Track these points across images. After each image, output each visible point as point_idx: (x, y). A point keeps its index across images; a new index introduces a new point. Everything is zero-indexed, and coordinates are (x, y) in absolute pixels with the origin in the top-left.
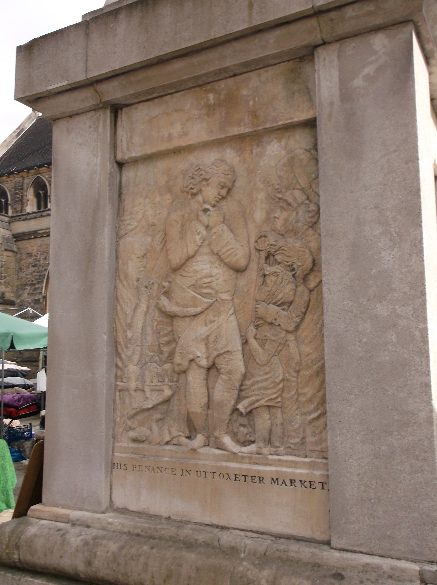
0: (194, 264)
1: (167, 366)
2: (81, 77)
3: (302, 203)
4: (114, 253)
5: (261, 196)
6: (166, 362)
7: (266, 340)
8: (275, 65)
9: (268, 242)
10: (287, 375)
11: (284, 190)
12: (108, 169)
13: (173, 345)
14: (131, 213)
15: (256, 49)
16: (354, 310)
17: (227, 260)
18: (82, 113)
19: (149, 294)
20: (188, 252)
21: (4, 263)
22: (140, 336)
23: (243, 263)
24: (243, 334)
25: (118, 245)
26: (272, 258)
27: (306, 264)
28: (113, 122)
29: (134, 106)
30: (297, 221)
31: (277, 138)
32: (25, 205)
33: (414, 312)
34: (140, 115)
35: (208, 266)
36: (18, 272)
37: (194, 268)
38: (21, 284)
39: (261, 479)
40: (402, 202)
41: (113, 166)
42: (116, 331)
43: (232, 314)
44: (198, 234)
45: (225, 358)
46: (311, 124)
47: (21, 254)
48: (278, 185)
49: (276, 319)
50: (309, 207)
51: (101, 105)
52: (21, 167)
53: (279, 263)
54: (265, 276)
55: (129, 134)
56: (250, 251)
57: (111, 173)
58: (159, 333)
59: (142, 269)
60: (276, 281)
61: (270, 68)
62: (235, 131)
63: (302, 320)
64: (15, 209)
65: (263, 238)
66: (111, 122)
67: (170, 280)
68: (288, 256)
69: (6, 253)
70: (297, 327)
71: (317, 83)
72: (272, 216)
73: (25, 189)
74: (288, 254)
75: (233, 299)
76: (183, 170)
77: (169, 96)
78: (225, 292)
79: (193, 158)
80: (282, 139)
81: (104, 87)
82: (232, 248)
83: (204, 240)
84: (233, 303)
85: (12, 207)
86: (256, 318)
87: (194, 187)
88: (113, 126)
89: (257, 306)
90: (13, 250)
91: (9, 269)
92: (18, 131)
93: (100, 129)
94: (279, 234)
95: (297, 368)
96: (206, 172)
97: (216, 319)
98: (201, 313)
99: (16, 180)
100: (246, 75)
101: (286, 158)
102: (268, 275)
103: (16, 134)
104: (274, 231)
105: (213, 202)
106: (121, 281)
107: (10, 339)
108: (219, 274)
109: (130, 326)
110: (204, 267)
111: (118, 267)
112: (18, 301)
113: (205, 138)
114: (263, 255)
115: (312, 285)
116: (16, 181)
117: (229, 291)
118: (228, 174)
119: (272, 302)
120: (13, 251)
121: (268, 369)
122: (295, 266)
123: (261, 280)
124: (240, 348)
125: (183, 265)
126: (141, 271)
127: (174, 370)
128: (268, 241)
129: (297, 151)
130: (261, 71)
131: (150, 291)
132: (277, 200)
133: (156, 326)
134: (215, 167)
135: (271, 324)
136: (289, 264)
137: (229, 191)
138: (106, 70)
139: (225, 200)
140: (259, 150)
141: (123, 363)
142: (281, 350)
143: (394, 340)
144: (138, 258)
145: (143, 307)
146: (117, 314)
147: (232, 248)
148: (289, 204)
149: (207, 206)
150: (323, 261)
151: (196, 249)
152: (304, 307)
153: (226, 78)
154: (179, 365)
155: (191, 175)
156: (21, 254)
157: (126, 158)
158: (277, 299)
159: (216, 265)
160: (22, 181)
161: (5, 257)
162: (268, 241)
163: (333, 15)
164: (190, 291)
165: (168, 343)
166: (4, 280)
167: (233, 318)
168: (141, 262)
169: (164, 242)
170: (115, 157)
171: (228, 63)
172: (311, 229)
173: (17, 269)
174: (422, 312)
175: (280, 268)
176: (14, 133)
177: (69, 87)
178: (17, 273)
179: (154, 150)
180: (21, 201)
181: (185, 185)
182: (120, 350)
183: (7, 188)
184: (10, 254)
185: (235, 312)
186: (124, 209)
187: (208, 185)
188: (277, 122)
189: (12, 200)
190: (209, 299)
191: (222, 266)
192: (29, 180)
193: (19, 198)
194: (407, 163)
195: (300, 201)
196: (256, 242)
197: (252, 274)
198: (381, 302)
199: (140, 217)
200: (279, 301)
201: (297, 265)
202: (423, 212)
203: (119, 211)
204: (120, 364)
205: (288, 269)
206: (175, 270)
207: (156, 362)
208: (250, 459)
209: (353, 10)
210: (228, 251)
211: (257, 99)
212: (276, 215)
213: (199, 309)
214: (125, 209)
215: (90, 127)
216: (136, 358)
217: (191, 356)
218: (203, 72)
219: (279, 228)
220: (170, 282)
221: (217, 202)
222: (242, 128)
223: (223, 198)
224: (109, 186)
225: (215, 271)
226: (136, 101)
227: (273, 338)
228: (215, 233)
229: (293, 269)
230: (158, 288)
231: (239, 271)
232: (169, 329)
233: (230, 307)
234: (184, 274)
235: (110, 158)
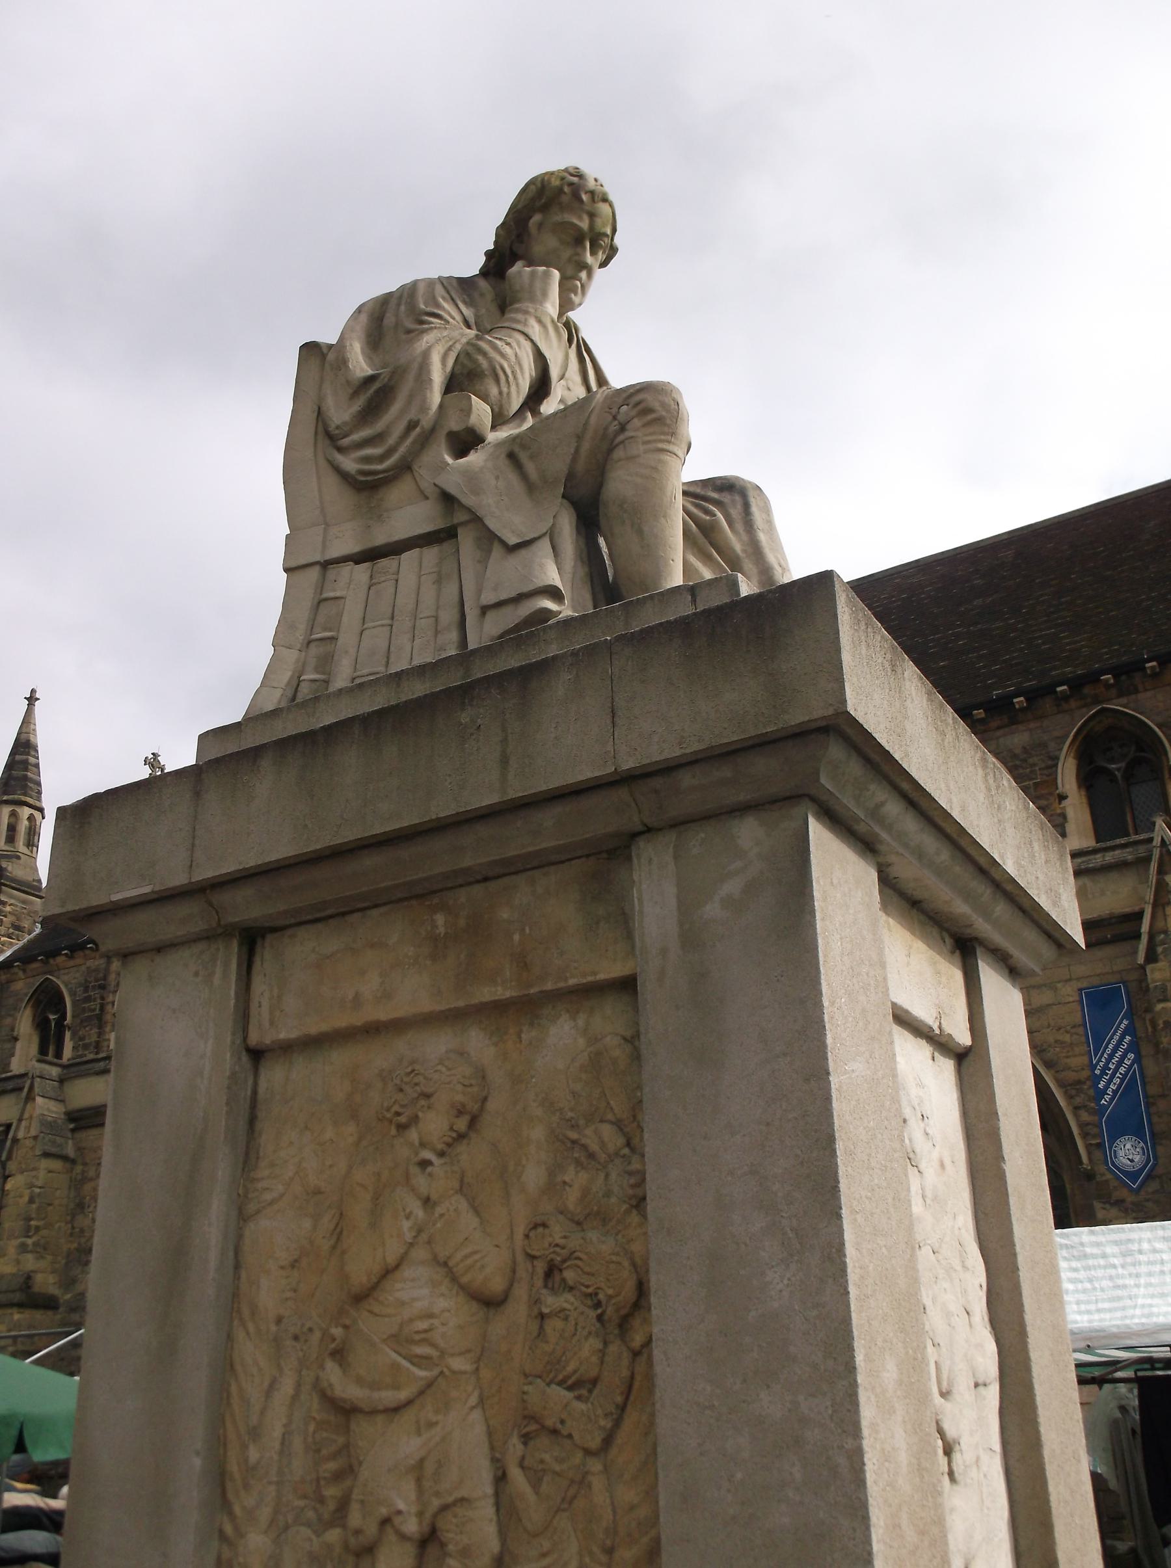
0: (398, 1286)
1: (334, 1535)
2: (179, 879)
3: (617, 1154)
4: (231, 1254)
5: (538, 1133)
6: (331, 1524)
7: (544, 1470)
8: (562, 862)
9: (550, 1239)
10: (587, 1560)
11: (582, 1122)
12: (228, 1066)
13: (348, 1483)
14: (272, 1165)
15: (519, 839)
16: (716, 1403)
17: (465, 1280)
18: (183, 944)
19: (301, 1354)
20: (384, 1258)
21: (37, 1190)
22: (276, 1457)
23: (497, 1285)
24: (498, 1455)
25: (240, 1236)
26: (557, 1277)
27: (623, 1294)
28: (245, 965)
29: (289, 932)
30: (608, 1194)
31: (568, 1011)
32: (108, 1029)
33: (834, 1411)
34: (303, 949)
35: (425, 1291)
36: (73, 1216)
37: (398, 1295)
38: (77, 1250)
40: (802, 1163)
41: (240, 1059)
42: (225, 1444)
43: (473, 1408)
44: (408, 1217)
45: (455, 1516)
46: (628, 985)
47: (85, 1164)
48: (572, 1110)
49: (562, 1422)
50: (630, 1163)
51: (220, 931)
53: (571, 1289)
54: (542, 1316)
55: (276, 991)
56: (514, 1256)
57: (233, 1076)
58: (318, 1451)
59: (289, 1294)
60: (563, 1330)
61: (553, 868)
62: (486, 994)
63: (617, 1423)
64: (81, 1039)
65: (540, 1230)
66: (239, 965)
67: (347, 1322)
68: (588, 1274)
69: (45, 1164)
70: (608, 1441)
71: (637, 908)
72: (559, 1179)
73: (112, 988)
74: (587, 1269)
75: (477, 1369)
76: (383, 1070)
77: (359, 914)
78: (461, 1354)
79: (402, 1046)
80: (578, 1012)
81: (224, 898)
82: (475, 1252)
83: (420, 1231)
84: (478, 1379)
85: (74, 1035)
86: (525, 1417)
87: (400, 1110)
88: (244, 973)
89: (526, 1388)
90: (64, 1152)
91: (51, 1208)
93: (217, 980)
94: (572, 1220)
95: (609, 1542)
96: (425, 1078)
97: (440, 1417)
98: (409, 1403)
99: (90, 963)
100: (506, 880)
101: (586, 1054)
102: (549, 1315)
104: (561, 1213)
105: (440, 1146)
106: (243, 1324)
107: (14, 1432)
108: (449, 1311)
109: (255, 1433)
110: (419, 1294)
111: (238, 1288)
112: (68, 1296)
113: (426, 1005)
114: (541, 1267)
115: (638, 1340)
116: (88, 968)
117: (469, 1351)
118: (471, 1085)
119: (556, 1380)
120: (64, 1158)
121: (546, 1545)
122: (601, 1296)
123: (534, 1327)
124: (490, 1490)
125: (375, 1287)
126: (287, 1299)
127: (346, 1546)
128: (551, 1235)
129: (608, 1038)
130: (536, 873)
131: (305, 1348)
132: (569, 1144)
133: (314, 1432)
134: (444, 1069)
135: (555, 1432)
136: (590, 1290)
137: (474, 1121)
138: (229, 867)
139: (465, 1141)
140: (533, 1034)
141: (236, 1528)
142: (575, 1497)
143: (798, 1476)
144: (282, 1268)
145: (287, 1387)
146: (229, 1404)
147: (475, 1252)
148: (592, 1156)
149: (427, 1155)
150: (653, 1290)
151: (402, 1251)
152: (622, 1393)
153: (470, 884)
154: (358, 1532)
155: (398, 1082)
156: (85, 1164)
157: (268, 1042)
158: (565, 1373)
159: (443, 1289)
160: (104, 966)
161: (42, 1174)
162: (551, 1235)
163: (657, 782)
164: (387, 1349)
165: (338, 1476)
166: (35, 1239)
167: (476, 1415)
168: (287, 1277)
169: (338, 1233)
170: (245, 1038)
171: (467, 861)
172: (635, 1212)
173: (72, 1206)
174: (849, 1411)
175: (572, 1299)
177: (156, 896)
178: (69, 1218)
179: (324, 1027)
180: (100, 1018)
181: (385, 1105)
182: (230, 1496)
183: (66, 986)
184: (57, 1165)
185: (481, 1401)
186: (258, 1153)
187: (429, 1107)
188: (566, 979)
189: (73, 1017)
190: (426, 1369)
191: (454, 1292)
193: (94, 1010)
194: (807, 1080)
195: (611, 1148)
196: (527, 1236)
197: (518, 1310)
198: (768, 1387)
199: (291, 1174)
200: (569, 1377)
201: (606, 1295)
202: (843, 1186)
203: (248, 1157)
204: (228, 1529)
205: (589, 1302)
206: (360, 1298)
207: (308, 1524)
209: (694, 777)
210: (466, 1257)
211: (527, 931)
212: (567, 1179)
213: (403, 1395)
214: (261, 1154)
215: (196, 974)
216: (265, 1514)
217: (384, 1511)
218: (421, 875)
219: (571, 1207)
220: (346, 1327)
221: (449, 1145)
222: (499, 988)
223: (461, 1137)
224: (227, 1104)
225: (442, 1303)
226: (293, 921)
227: (557, 1468)
228: (442, 1215)
229: (598, 1304)
230: (322, 1340)
231: (491, 1303)
232: (341, 1440)
233: (470, 1388)
234: (377, 1309)
235: (233, 1043)
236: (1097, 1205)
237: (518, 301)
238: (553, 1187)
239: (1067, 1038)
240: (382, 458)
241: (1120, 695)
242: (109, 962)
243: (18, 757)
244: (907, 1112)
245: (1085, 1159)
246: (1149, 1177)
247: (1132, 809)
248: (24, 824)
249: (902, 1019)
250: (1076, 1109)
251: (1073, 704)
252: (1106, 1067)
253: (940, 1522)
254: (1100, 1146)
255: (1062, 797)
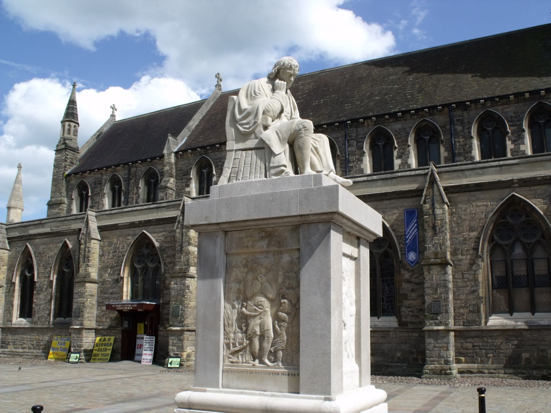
5: (281, 273)
39: (278, 374)
52: (100, 166)
92: (98, 134)
99: (96, 176)
103: (96, 136)
114: (281, 295)
176: (94, 135)
192: (106, 176)
208: (274, 367)
236: (402, 270)
237: (277, 89)
238: (283, 282)
239: (399, 223)
240: (248, 128)
241: (430, 115)
242: (102, 176)
243: (70, 106)
244: (343, 271)
245: (400, 257)
246: (417, 263)
247: (430, 154)
248: (72, 129)
249: (345, 255)
250: (399, 243)
251: (415, 117)
252: (409, 232)
253: (342, 334)
254: (405, 254)
255: (409, 146)
